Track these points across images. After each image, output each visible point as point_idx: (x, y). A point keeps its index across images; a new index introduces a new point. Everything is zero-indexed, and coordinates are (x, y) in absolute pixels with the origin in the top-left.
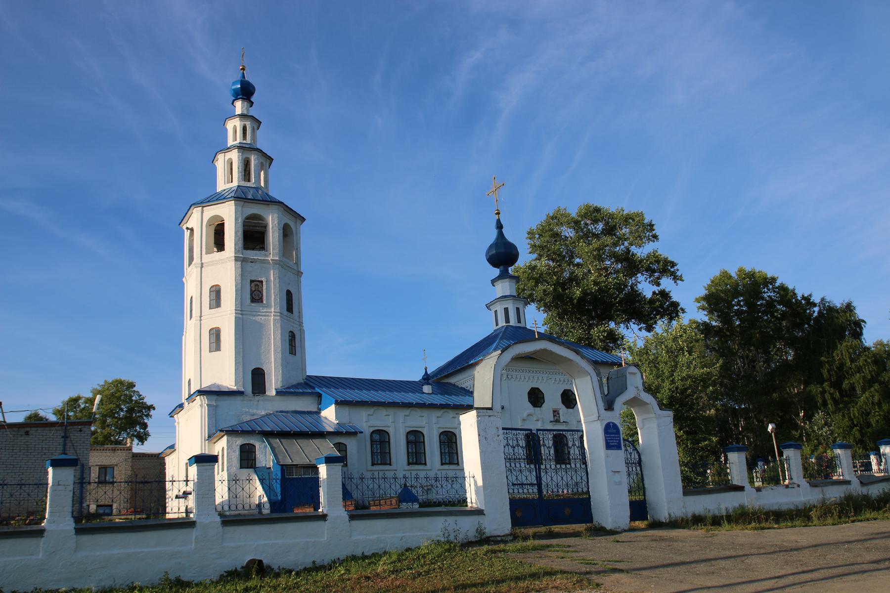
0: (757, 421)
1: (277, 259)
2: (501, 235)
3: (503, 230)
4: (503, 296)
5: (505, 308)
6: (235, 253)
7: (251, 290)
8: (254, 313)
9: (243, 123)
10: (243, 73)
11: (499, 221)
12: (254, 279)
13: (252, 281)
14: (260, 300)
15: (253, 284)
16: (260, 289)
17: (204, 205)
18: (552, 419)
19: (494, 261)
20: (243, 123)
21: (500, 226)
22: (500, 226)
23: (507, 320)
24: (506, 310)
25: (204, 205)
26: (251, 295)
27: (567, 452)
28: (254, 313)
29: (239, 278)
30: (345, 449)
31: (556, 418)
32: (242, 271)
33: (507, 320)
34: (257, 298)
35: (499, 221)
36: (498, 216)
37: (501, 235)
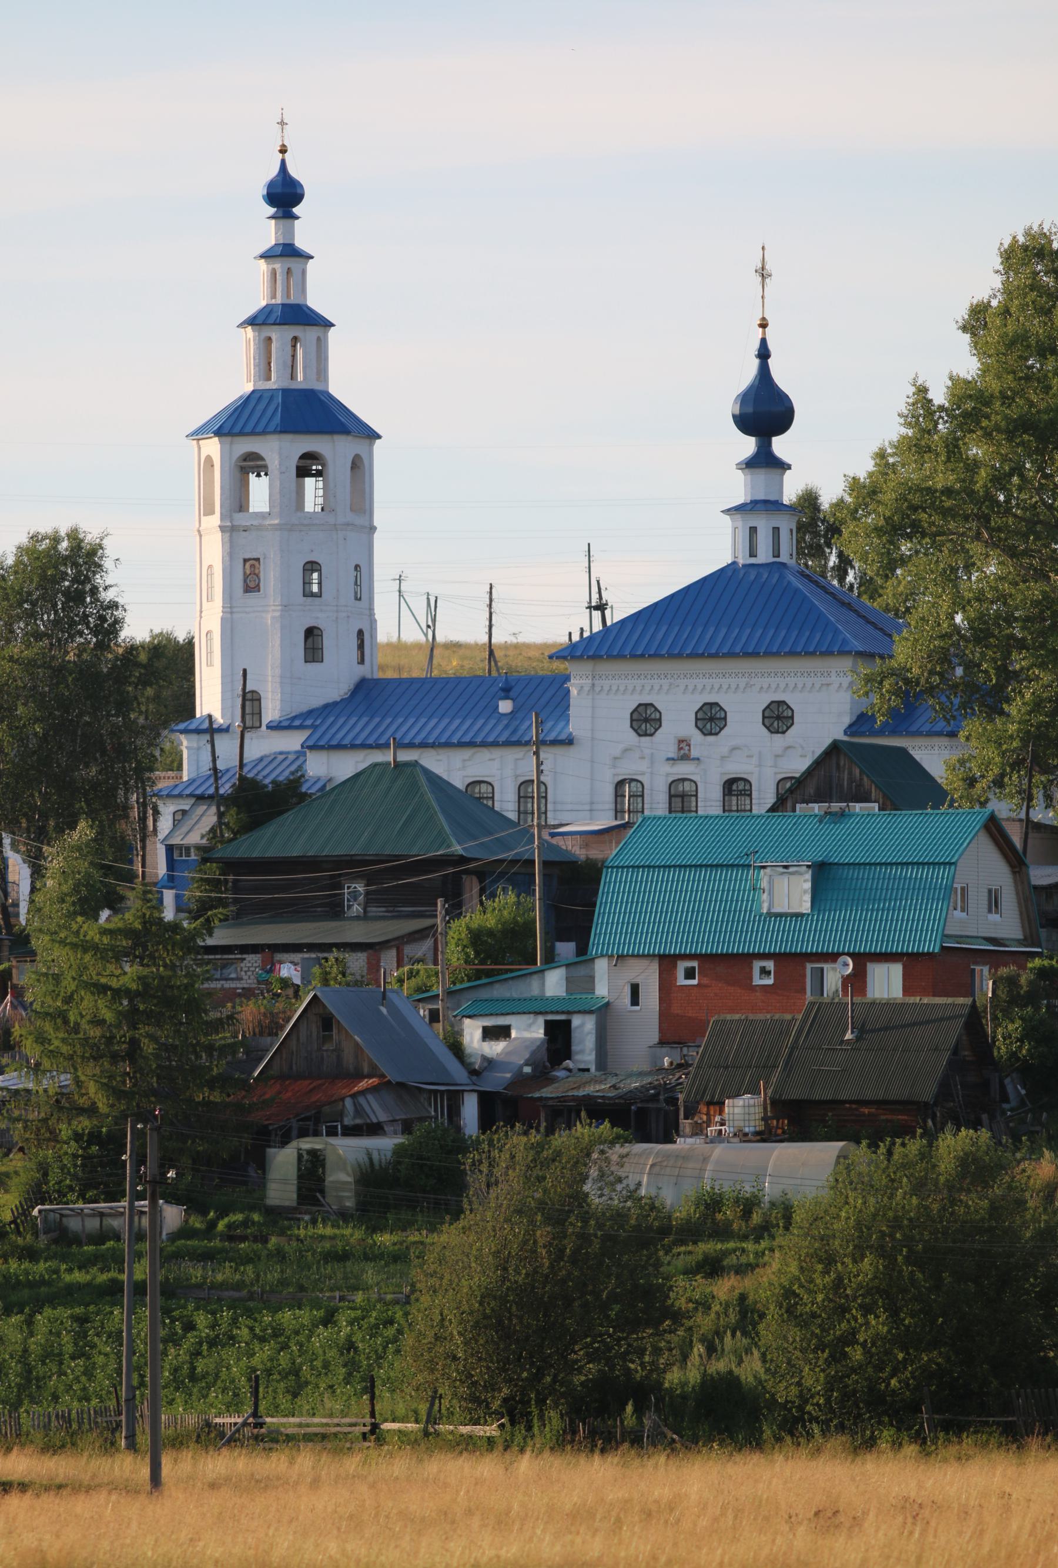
0: (73, 828)
1: (276, 522)
2: (764, 372)
3: (769, 361)
4: (766, 502)
5: (774, 528)
6: (221, 520)
7: (245, 573)
8: (247, 610)
9: (271, 267)
10: (283, 162)
11: (764, 342)
12: (247, 556)
13: (245, 561)
14: (257, 588)
15: (248, 565)
16: (257, 571)
17: (200, 437)
18: (671, 755)
19: (745, 423)
20: (271, 267)
21: (764, 354)
22: (764, 354)
23: (777, 554)
24: (776, 530)
25: (200, 437)
26: (245, 581)
27: (151, 829)
28: (247, 610)
29: (227, 558)
30: (673, 799)
31: (682, 752)
32: (231, 547)
33: (777, 554)
34: (252, 585)
35: (764, 342)
36: (764, 333)
37: (764, 372)
